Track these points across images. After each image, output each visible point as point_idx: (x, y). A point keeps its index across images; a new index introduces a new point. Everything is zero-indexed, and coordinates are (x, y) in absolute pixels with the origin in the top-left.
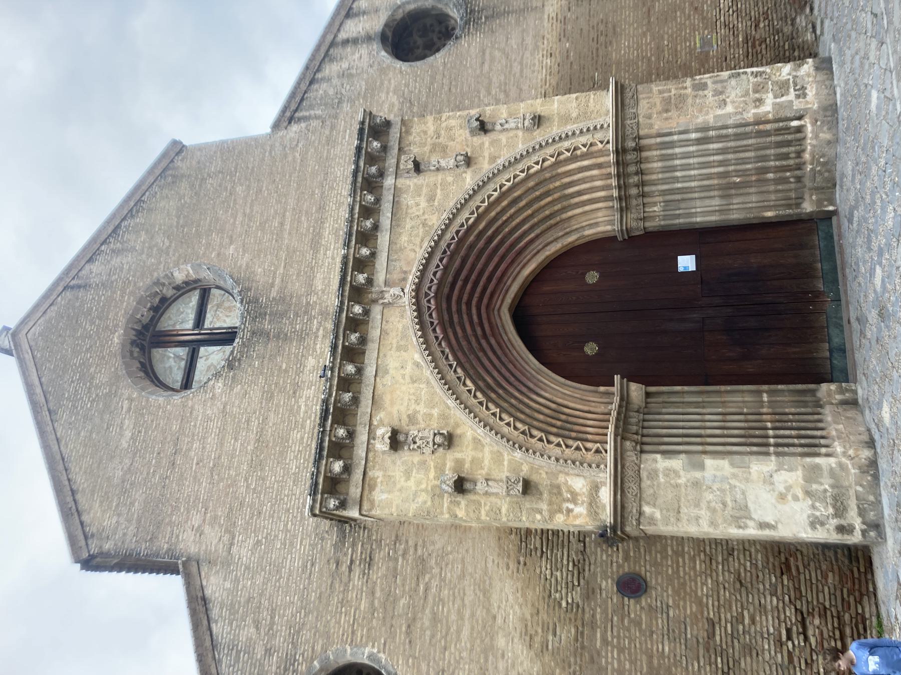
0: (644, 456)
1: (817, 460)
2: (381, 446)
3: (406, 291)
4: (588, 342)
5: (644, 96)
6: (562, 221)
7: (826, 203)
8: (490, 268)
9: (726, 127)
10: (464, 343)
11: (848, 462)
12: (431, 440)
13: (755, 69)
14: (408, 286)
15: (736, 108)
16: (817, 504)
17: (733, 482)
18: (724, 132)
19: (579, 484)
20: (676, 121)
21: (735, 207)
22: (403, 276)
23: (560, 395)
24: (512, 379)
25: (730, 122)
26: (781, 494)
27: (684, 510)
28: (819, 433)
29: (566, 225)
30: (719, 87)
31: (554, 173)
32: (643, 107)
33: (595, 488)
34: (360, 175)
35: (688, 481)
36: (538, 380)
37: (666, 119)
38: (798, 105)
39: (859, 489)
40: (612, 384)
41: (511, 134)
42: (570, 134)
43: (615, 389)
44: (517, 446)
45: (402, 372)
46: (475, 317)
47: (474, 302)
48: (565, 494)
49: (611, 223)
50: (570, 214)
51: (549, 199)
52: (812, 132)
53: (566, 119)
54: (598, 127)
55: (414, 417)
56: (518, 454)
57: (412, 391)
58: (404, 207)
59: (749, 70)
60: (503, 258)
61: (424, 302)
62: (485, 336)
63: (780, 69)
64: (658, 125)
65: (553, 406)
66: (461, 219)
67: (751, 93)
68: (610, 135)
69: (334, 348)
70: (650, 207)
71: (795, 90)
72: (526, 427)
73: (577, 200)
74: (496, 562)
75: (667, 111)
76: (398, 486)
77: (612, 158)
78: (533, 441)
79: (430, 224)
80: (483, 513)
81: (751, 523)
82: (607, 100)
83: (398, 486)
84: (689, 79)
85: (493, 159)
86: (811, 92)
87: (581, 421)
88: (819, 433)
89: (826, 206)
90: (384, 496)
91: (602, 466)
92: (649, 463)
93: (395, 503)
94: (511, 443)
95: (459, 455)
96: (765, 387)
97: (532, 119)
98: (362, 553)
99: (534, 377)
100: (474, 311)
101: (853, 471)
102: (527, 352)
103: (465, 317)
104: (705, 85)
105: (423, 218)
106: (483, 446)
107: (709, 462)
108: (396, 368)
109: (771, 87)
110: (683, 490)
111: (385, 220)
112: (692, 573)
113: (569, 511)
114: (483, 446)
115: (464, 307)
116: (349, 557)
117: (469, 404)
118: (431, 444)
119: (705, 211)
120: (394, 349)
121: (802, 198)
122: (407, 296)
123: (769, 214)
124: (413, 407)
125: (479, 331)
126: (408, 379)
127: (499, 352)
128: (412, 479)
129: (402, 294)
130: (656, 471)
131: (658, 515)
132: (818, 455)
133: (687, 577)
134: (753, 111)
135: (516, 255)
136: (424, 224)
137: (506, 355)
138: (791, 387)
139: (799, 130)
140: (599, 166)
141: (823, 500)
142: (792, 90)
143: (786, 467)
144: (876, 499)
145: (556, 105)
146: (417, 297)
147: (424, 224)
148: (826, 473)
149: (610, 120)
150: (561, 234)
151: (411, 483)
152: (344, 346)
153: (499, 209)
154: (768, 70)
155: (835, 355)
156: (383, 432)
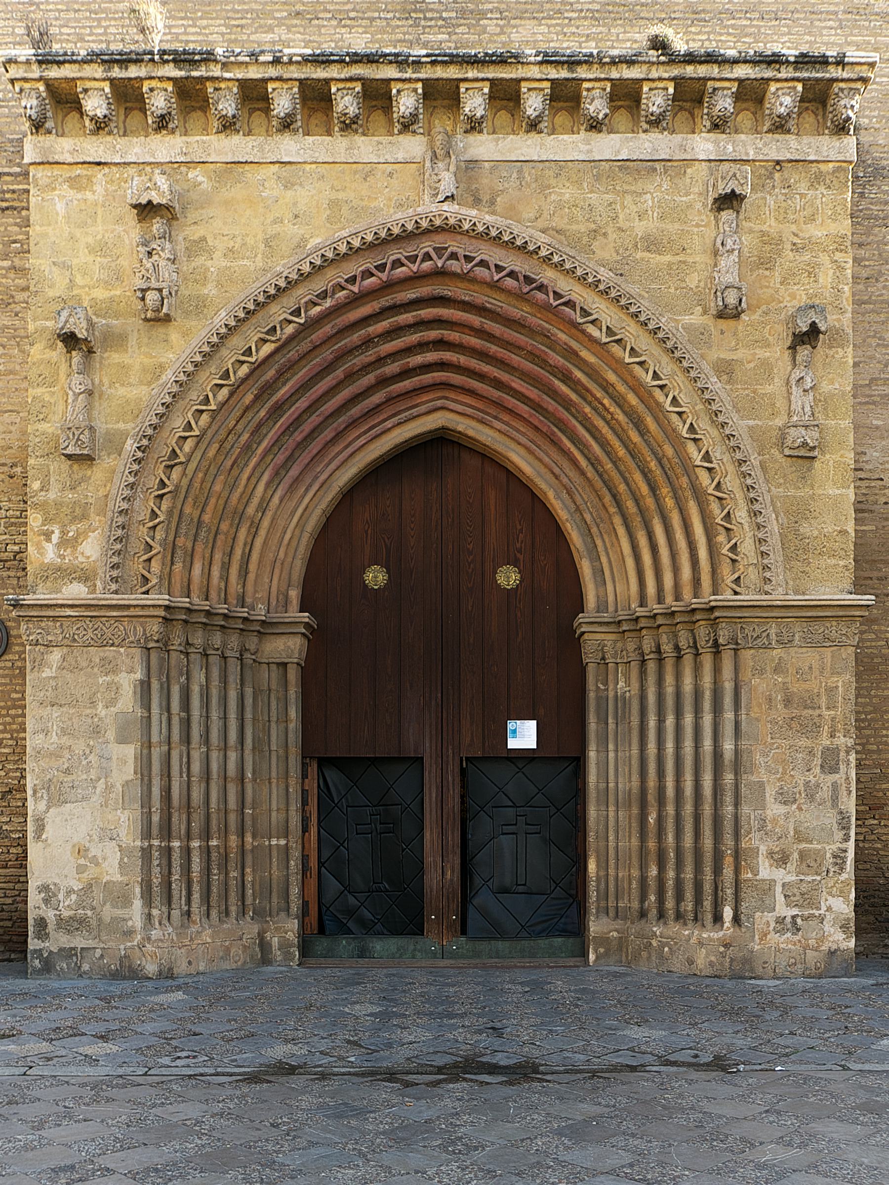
0: (137, 652)
1: (138, 904)
2: (136, 189)
3: (445, 206)
5: (828, 660)
8: (517, 384)
9: (737, 804)
10: (356, 337)
12: (154, 284)
13: (851, 855)
14: (464, 211)
15: (775, 820)
16: (74, 897)
17: (101, 785)
18: (729, 798)
19: (92, 549)
20: (763, 714)
21: (611, 814)
22: (485, 198)
24: (298, 436)
25: (745, 809)
26: (87, 850)
27: (56, 713)
30: (825, 793)
32: (804, 657)
33: (86, 577)
34: (714, 71)
35: (100, 719)
36: (310, 486)
37: (770, 700)
38: (764, 919)
39: (98, 953)
40: (302, 610)
41: (780, 403)
42: (760, 520)
44: (145, 442)
46: (418, 360)
48: (74, 527)
49: (602, 606)
51: (644, 489)
52: (710, 939)
53: (799, 512)
54: (768, 574)
56: (130, 445)
57: (250, 241)
58: (639, 186)
59: (851, 845)
60: (537, 407)
61: (426, 246)
62: (384, 382)
63: (842, 894)
64: (759, 685)
67: (803, 845)
68: (747, 597)
69: (321, 60)
70: (624, 675)
71: (793, 917)
72: (182, 459)
74: (13, 428)
75: (787, 702)
76: (78, 233)
77: (707, 597)
78: (160, 472)
79: (596, 245)
80: (39, 391)
81: (42, 806)
82: (832, 586)
83: (78, 233)
84: (850, 742)
85: (726, 369)
86: (785, 941)
89: (596, 951)
90: (60, 207)
91: (114, 587)
92: (127, 661)
93: (50, 230)
97: (805, 444)
98: (14, 192)
99: (316, 478)
100: (431, 357)
103: (413, 338)
104: (834, 770)
105: (610, 230)
106: (149, 384)
107: (130, 751)
108: (295, 204)
109: (809, 878)
110: (88, 711)
111: (609, 146)
112: (14, 727)
113: (48, 536)
114: (149, 384)
115: (433, 334)
116: (6, 170)
117: (224, 352)
119: (609, 768)
120: (334, 196)
121: (617, 916)
123: (592, 866)
124: (220, 245)
125: (392, 368)
126: (272, 230)
127: (356, 411)
128: (90, 259)
129: (441, 197)
130: (115, 671)
131: (47, 673)
132: (148, 901)
133: (8, 719)
134: (763, 849)
136: (594, 233)
137: (354, 423)
139: (718, 918)
140: (696, 582)
141: (80, 905)
142: (795, 911)
143: (126, 860)
144: (84, 973)
145: (832, 491)
146: (433, 230)
147: (594, 233)
148: (119, 912)
149: (778, 596)
151: (83, 258)
152: (327, 82)
154: (844, 876)
156: (161, 190)
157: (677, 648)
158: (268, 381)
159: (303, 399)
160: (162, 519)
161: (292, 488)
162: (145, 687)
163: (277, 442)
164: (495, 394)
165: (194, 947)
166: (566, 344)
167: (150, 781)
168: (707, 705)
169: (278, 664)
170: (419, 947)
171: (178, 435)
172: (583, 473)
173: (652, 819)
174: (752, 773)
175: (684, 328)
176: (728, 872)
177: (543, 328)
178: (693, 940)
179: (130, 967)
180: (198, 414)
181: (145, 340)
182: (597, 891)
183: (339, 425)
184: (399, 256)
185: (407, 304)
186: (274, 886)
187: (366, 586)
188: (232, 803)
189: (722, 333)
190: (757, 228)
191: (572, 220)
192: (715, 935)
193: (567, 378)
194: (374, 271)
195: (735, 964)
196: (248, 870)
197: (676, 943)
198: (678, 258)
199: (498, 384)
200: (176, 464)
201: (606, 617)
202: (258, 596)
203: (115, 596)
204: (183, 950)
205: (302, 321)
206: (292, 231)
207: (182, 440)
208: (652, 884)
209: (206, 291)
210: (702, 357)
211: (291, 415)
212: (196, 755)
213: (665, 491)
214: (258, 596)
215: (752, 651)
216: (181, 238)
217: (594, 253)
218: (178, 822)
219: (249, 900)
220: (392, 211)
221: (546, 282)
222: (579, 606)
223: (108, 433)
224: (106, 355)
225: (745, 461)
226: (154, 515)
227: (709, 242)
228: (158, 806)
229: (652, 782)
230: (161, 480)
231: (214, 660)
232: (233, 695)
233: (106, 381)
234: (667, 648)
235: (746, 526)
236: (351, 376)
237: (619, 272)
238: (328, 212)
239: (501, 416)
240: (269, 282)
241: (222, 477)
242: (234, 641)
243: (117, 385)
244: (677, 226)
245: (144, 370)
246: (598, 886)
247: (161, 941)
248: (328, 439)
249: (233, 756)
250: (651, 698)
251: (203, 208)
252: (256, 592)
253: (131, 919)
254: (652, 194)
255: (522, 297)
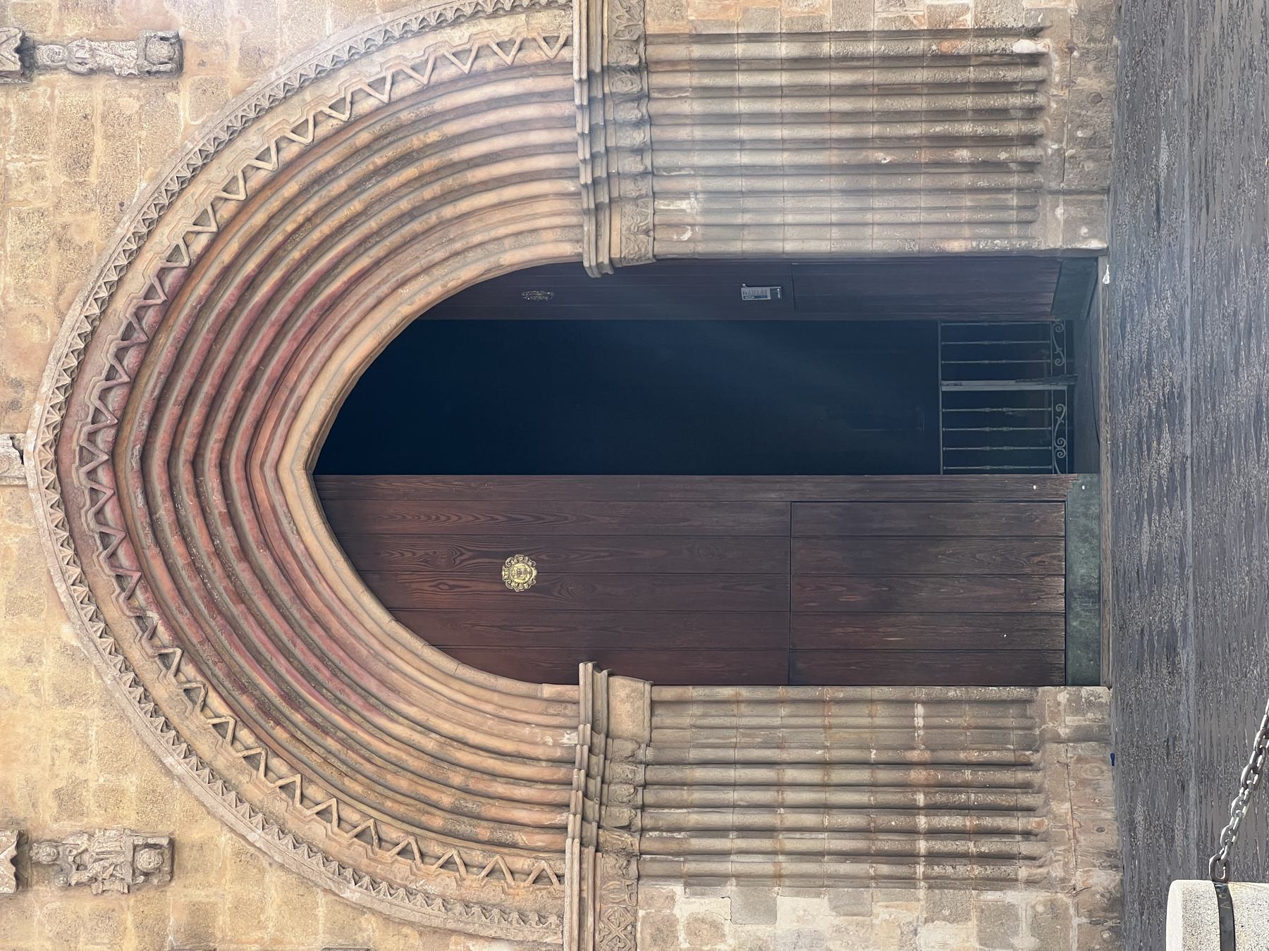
0: (646, 889)
1: (1012, 897)
3: (28, 448)
4: (512, 554)
6: (444, 223)
7: (1084, 230)
10: (191, 583)
11: (1069, 901)
18: (857, 48)
23: (443, 707)
24: (323, 675)
28: (1018, 823)
29: (453, 232)
31: (424, 110)
36: (388, 664)
43: (580, 692)
44: (348, 873)
45: (28, 671)
46: (216, 499)
47: (211, 456)
50: (464, 206)
51: (410, 172)
55: (71, 796)
57: (61, 727)
61: (78, 477)
62: (244, 552)
65: (430, 743)
66: (166, 237)
73: (481, 174)
87: (499, 788)
88: (1018, 823)
89: (1085, 239)
91: (553, 919)
94: (335, 865)
95: (199, 895)
96: (922, 692)
99: (377, 655)
101: (1076, 921)
102: (358, 588)
105: (60, 220)
106: (262, 871)
108: (11, 662)
118: (127, 873)
122: (30, 463)
124: (66, 768)
126: (48, 694)
127: (285, 595)
130: (671, 923)
132: (1007, 882)
135: (320, 315)
136: (62, 242)
137: (299, 597)
138: (977, 692)
139: (1033, 59)
148: (1024, 926)
150: (440, 255)
153: (274, 204)
155: (1077, 607)
157: (638, 124)
158: (257, 705)
159: (274, 662)
160: (454, 852)
161: (394, 690)
162: (695, 882)
163: (337, 702)
164: (262, 389)
165: (1076, 824)
166: (212, 284)
167: (830, 877)
168: (723, 81)
169: (652, 715)
170: (1081, 509)
171: (336, 829)
172: (377, 264)
173: (884, 157)
174: (821, 17)
175: (197, 118)
176: (964, 46)
177: (189, 316)
178: (1064, 94)
179: (1105, 910)
180: (306, 802)
181: (200, 876)
182: (994, 238)
183: (304, 617)
184: (90, 514)
185: (149, 508)
186: (986, 722)
187: (533, 588)
188: (863, 775)
189: (202, 64)
190: (55, 16)
191: (44, 273)
192: (1057, 64)
193: (251, 284)
194: (110, 550)
195: (1096, 34)
196: (962, 756)
197: (1070, 121)
198: (98, 124)
199: (250, 386)
200: (377, 832)
201: (589, 227)
202: (550, 740)
203: (567, 916)
204: (1081, 838)
205: (179, 652)
206: (49, 667)
207: (344, 825)
208: (983, 154)
209: (133, 789)
210: (239, 92)
211: (297, 680)
212: (792, 819)
213: (416, 142)
214: (550, 740)
215: (649, 20)
216: (55, 826)
217: (90, 243)
218: (887, 843)
219: (1009, 757)
220: (26, 525)
221: (131, 310)
222: (572, 268)
223: (330, 932)
224: (219, 935)
225: (386, 32)
226: (448, 864)
227: (75, 82)
228: (867, 866)
229: (833, 157)
230: (399, 854)
231: (650, 796)
232: (700, 774)
233: (256, 935)
234: (638, 137)
235: (474, 30)
236: (240, 596)
237: (118, 208)
238: (25, 615)
239: (290, 384)
240: (125, 696)
241: (389, 777)
242: (620, 770)
243: (262, 918)
244: (52, 127)
245: (242, 878)
246: (987, 238)
247: (1066, 864)
248: (322, 632)
249: (791, 774)
250: (710, 160)
251: (12, 795)
252: (545, 744)
253: (1033, 907)
254: (7, 162)
255: (149, 345)
